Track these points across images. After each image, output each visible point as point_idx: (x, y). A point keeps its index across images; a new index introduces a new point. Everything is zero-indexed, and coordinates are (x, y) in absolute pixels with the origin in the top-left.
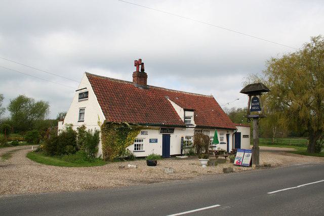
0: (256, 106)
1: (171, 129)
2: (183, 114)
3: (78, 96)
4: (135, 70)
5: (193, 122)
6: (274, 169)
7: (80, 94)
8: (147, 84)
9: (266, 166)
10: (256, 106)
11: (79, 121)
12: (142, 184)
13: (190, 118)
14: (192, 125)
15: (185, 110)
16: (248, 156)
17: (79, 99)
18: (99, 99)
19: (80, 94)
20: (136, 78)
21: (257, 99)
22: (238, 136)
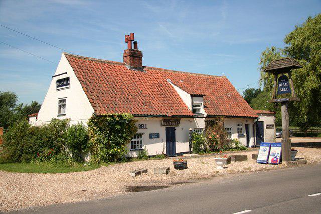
0: (283, 87)
10: (283, 87)
11: (58, 116)
15: (192, 96)
17: (57, 87)
19: (58, 81)
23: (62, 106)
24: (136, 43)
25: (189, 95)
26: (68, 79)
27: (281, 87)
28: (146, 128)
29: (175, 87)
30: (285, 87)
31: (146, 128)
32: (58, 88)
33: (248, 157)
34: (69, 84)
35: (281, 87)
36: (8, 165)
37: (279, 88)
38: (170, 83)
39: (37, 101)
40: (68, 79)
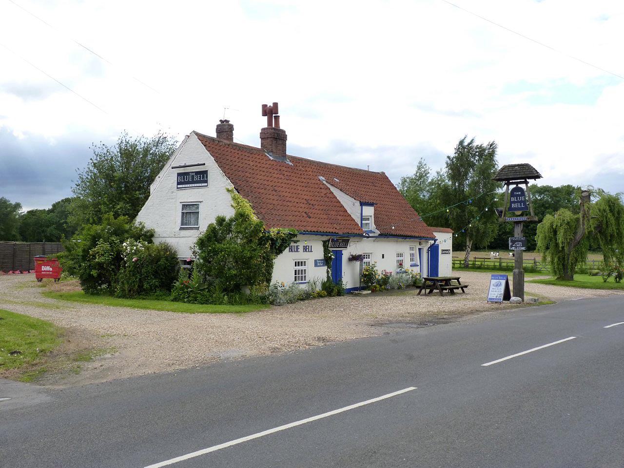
0: (518, 202)
1: (343, 241)
2: (360, 212)
3: (175, 178)
4: (265, 125)
5: (372, 227)
6: (328, 343)
7: (179, 175)
8: (235, 141)
9: (537, 302)
10: (518, 202)
11: (181, 229)
12: (423, 332)
13: (368, 219)
14: (371, 232)
15: (362, 204)
16: (498, 285)
17: (178, 184)
18: (330, 195)
19: (179, 175)
20: (269, 140)
21: (521, 189)
22: (434, 251)
23: (185, 214)
24: (277, 118)
25: (358, 204)
26: (205, 173)
27: (514, 202)
28: (311, 251)
29: (332, 189)
30: (521, 202)
31: (311, 251)
32: (179, 186)
33: (507, 302)
34: (206, 182)
35: (514, 202)
36: (327, 299)
37: (512, 203)
38: (325, 182)
39: (221, 215)
40: (205, 173)
